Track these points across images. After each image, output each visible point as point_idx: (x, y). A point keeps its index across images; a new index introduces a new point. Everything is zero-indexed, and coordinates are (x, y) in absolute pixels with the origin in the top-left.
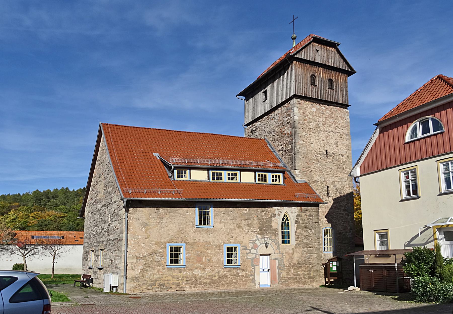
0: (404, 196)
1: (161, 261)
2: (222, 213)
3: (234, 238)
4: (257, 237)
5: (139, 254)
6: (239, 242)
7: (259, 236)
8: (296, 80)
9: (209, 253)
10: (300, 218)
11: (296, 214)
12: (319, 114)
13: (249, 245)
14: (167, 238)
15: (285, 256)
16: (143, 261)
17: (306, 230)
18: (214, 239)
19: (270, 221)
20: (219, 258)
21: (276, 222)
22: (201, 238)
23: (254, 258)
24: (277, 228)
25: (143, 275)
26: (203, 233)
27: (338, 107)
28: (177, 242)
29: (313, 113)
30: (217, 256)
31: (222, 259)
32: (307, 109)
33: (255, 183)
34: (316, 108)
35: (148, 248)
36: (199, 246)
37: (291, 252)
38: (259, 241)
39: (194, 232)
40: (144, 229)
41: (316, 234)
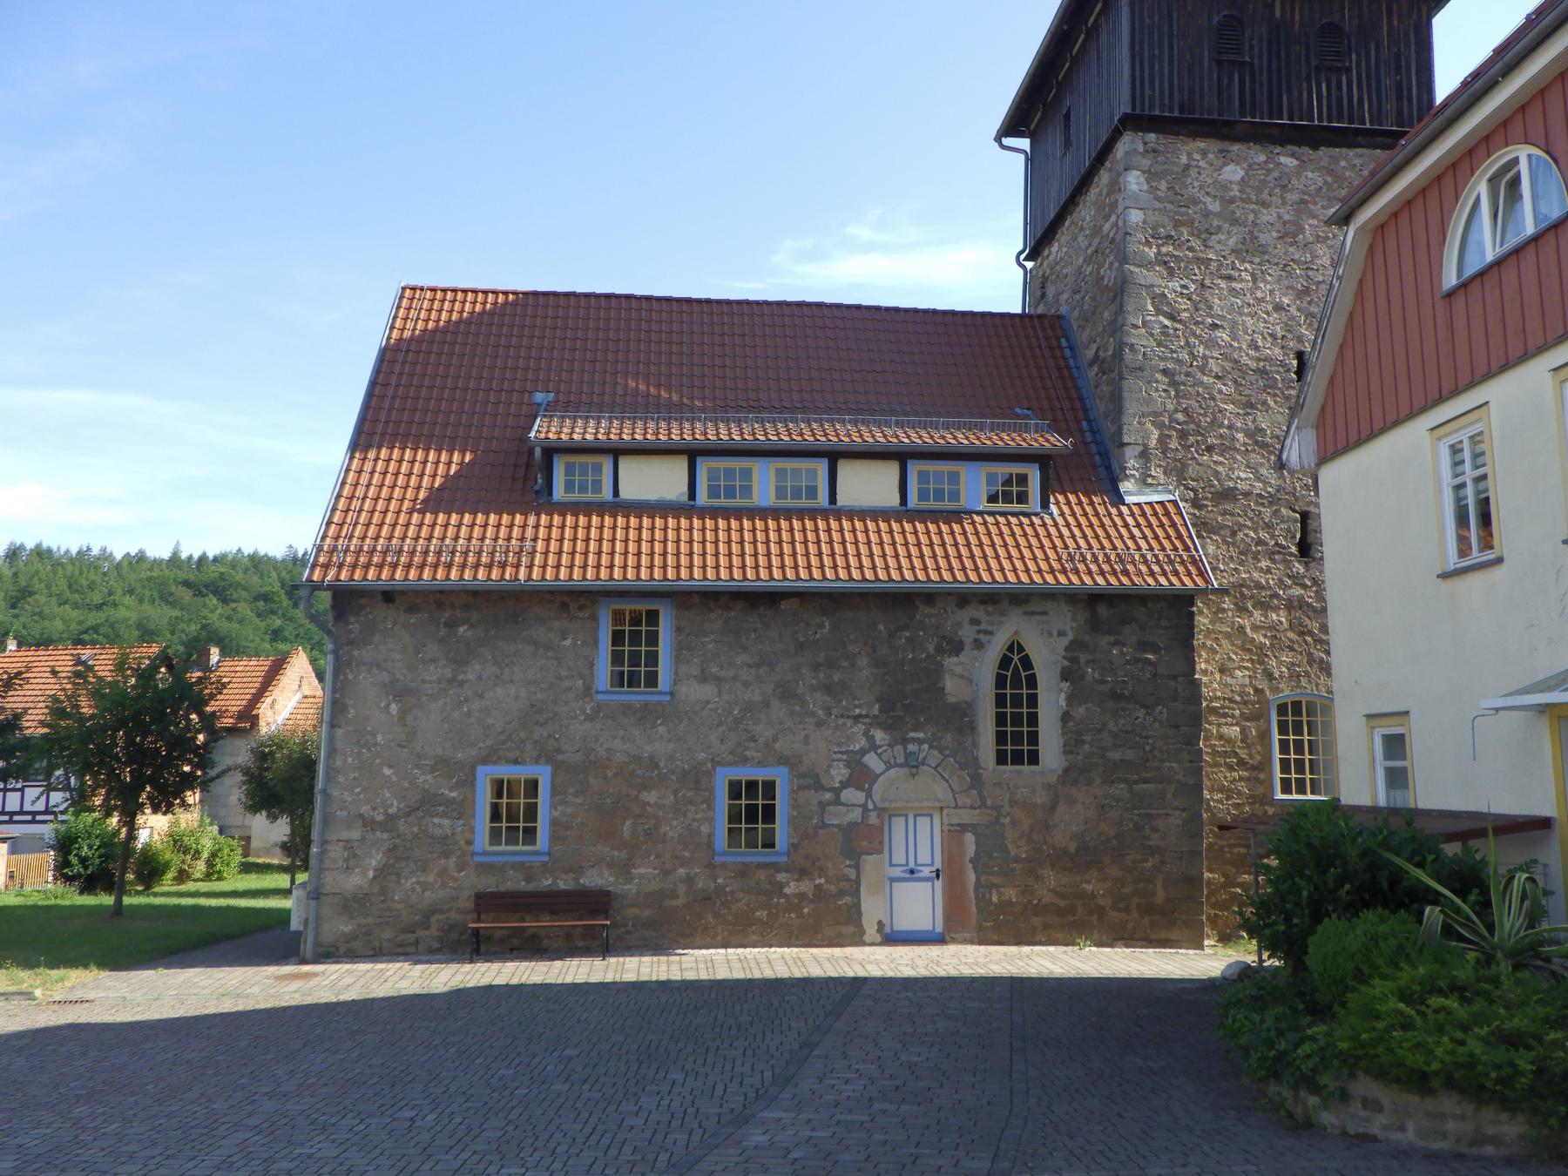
0: (1453, 560)
1: (453, 834)
2: (712, 637)
3: (761, 741)
4: (871, 739)
5: (374, 809)
6: (782, 760)
7: (879, 735)
8: (1137, 48)
9: (648, 804)
10: (1083, 658)
11: (1065, 642)
12: (1259, 190)
13: (833, 772)
14: (481, 745)
15: (1008, 819)
16: (386, 836)
17: (1123, 709)
18: (671, 746)
19: (939, 671)
20: (696, 824)
21: (962, 676)
22: (617, 744)
23: (853, 825)
24: (968, 699)
25: (384, 891)
26: (626, 721)
27: (1375, 148)
28: (516, 762)
29: (1225, 187)
30: (685, 814)
31: (705, 829)
32: (1193, 172)
33: (903, 508)
34: (1245, 165)
35: (406, 784)
36: (610, 774)
37: (1040, 798)
38: (879, 756)
39: (589, 718)
40: (394, 708)
41: (1176, 727)
